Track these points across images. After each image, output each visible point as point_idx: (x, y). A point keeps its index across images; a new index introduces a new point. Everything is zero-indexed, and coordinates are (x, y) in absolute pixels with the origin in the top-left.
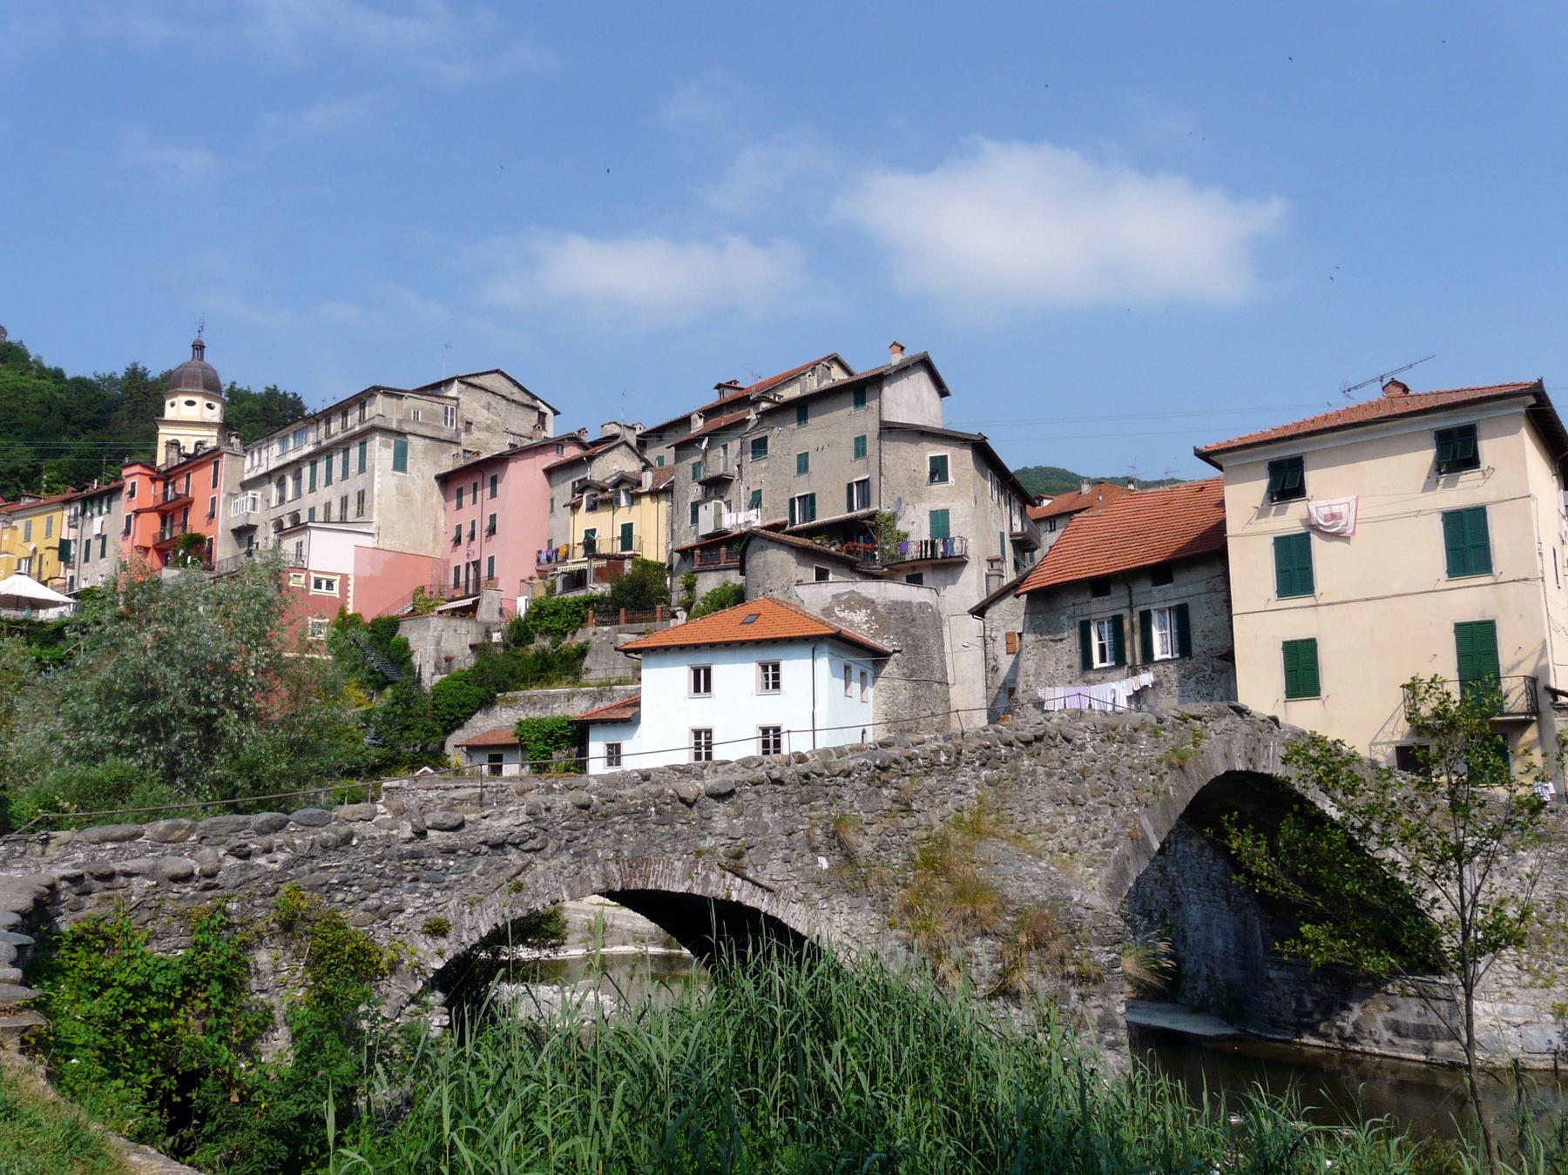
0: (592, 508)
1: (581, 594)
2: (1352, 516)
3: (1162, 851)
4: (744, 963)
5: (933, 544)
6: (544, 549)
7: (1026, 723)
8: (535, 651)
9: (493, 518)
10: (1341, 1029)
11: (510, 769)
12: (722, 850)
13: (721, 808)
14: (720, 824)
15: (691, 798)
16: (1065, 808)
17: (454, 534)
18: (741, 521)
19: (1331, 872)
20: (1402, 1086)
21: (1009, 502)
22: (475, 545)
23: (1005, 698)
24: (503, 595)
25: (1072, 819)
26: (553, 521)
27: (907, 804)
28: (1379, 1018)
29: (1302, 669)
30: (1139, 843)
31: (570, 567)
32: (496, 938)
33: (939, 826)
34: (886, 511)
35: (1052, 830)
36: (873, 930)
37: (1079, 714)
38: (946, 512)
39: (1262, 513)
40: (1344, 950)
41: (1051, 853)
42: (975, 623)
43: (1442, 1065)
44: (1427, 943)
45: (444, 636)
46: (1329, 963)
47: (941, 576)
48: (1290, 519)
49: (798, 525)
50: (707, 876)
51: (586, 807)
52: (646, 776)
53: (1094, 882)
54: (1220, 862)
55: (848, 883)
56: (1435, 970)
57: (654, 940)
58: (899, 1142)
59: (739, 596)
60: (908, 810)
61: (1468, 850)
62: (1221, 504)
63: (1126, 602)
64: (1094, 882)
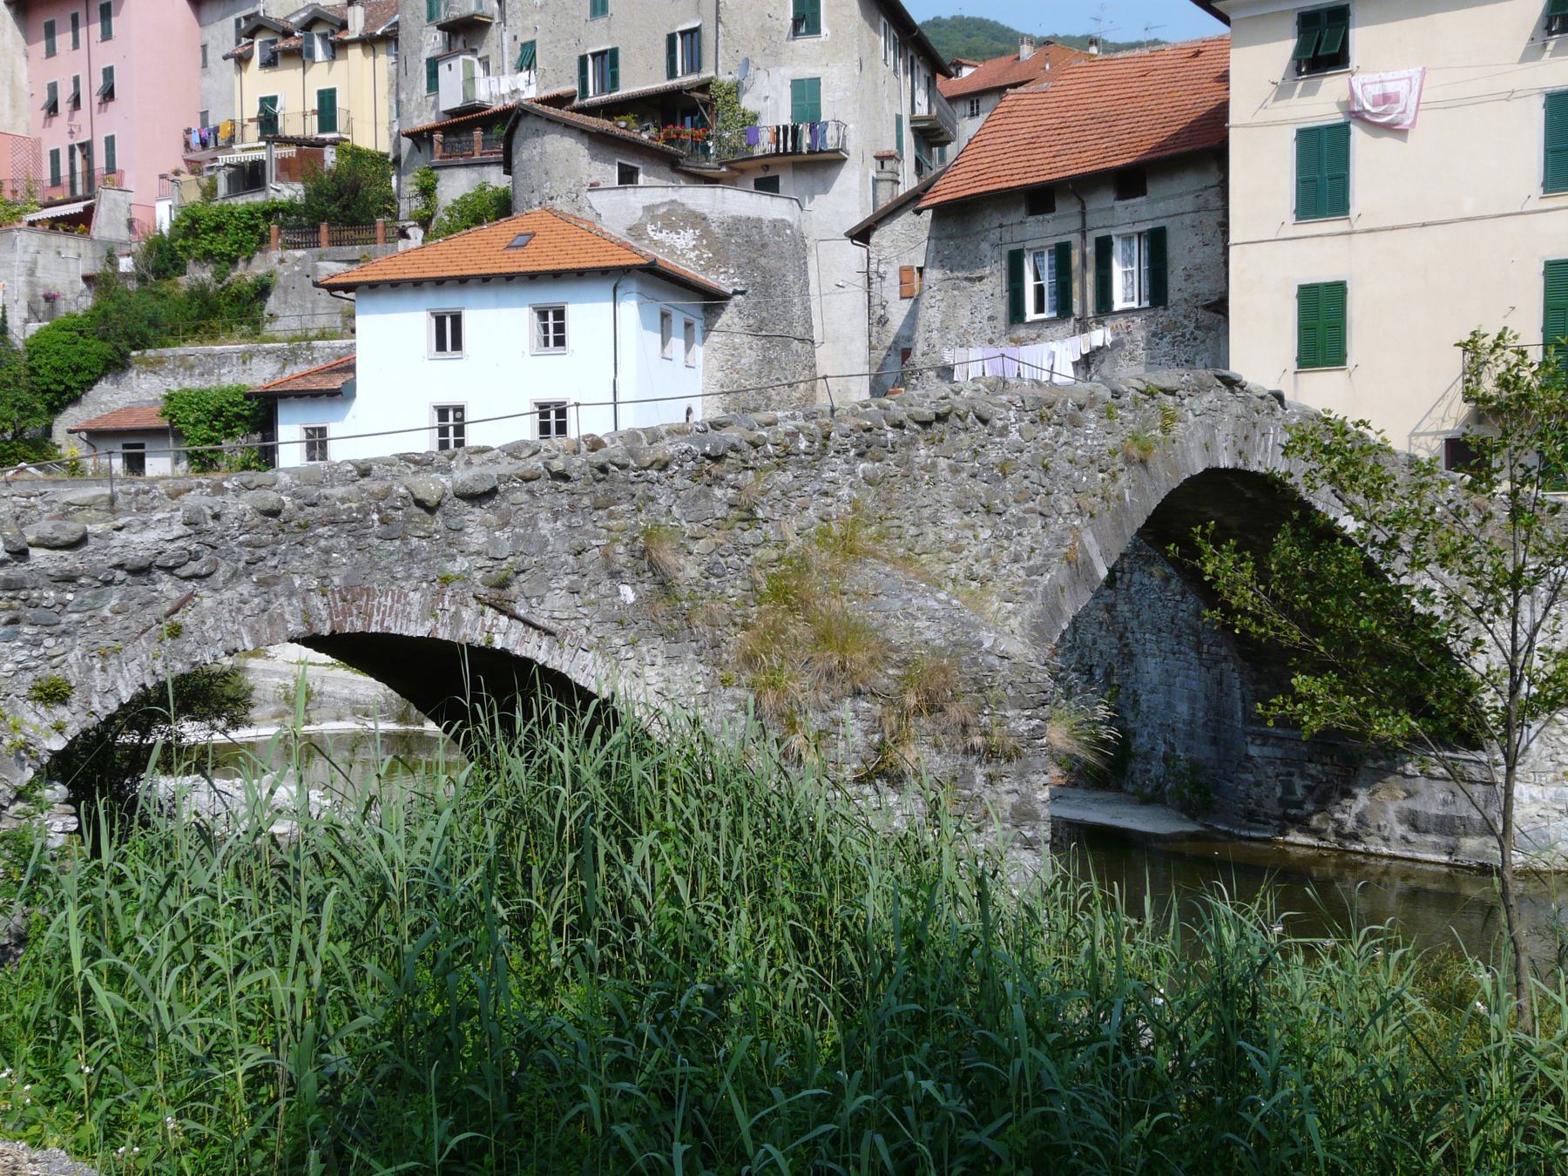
0: (270, 63)
1: (257, 199)
2: (1414, 99)
3: (1111, 581)
4: (511, 734)
5: (795, 131)
6: (196, 125)
7: (926, 396)
8: (192, 281)
9: (108, 73)
10: (1340, 823)
11: (158, 465)
12: (479, 575)
13: (476, 516)
14: (476, 537)
15: (433, 499)
16: (977, 519)
17: (44, 97)
18: (505, 90)
19: (1341, 604)
20: (1414, 896)
21: (911, 69)
22: (82, 115)
23: (896, 362)
24: (132, 198)
25: (985, 534)
26: (207, 83)
27: (750, 510)
28: (1392, 808)
29: (1322, 325)
30: (1079, 567)
31: (239, 155)
32: (144, 710)
33: (795, 543)
34: (725, 78)
35: (958, 550)
36: (701, 688)
37: (1002, 384)
38: (815, 82)
39: (1283, 91)
40: (1350, 708)
41: (954, 580)
42: (856, 252)
43: (1469, 868)
44: (1460, 701)
45: (41, 262)
46: (1328, 727)
47: (805, 180)
48: (1323, 101)
49: (593, 98)
50: (457, 614)
51: (274, 513)
52: (364, 471)
53: (1014, 623)
54: (1191, 599)
55: (664, 623)
56: (1472, 742)
57: (385, 714)
58: (732, 969)
59: (503, 206)
60: (750, 518)
61: (1528, 575)
62: (1224, 78)
63: (1076, 224)
64: (1014, 623)
